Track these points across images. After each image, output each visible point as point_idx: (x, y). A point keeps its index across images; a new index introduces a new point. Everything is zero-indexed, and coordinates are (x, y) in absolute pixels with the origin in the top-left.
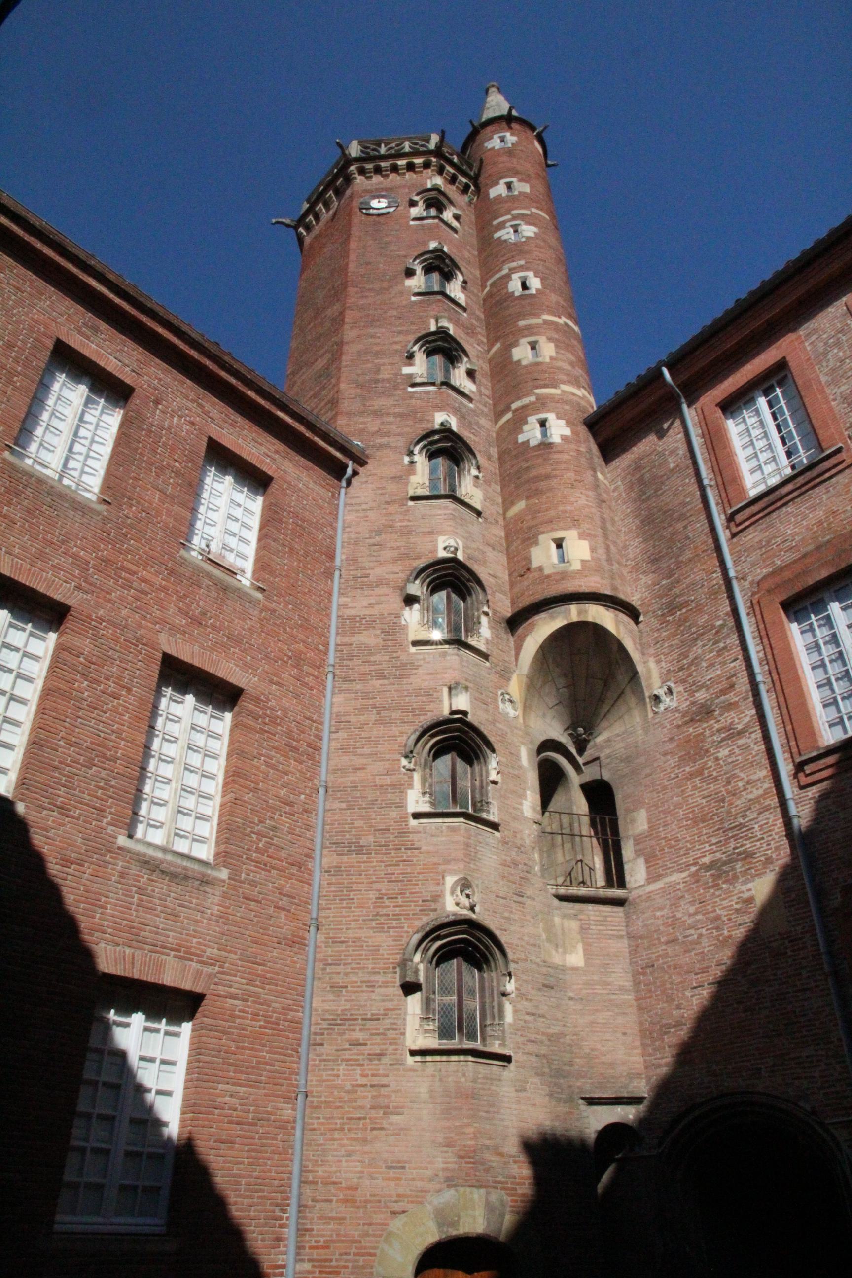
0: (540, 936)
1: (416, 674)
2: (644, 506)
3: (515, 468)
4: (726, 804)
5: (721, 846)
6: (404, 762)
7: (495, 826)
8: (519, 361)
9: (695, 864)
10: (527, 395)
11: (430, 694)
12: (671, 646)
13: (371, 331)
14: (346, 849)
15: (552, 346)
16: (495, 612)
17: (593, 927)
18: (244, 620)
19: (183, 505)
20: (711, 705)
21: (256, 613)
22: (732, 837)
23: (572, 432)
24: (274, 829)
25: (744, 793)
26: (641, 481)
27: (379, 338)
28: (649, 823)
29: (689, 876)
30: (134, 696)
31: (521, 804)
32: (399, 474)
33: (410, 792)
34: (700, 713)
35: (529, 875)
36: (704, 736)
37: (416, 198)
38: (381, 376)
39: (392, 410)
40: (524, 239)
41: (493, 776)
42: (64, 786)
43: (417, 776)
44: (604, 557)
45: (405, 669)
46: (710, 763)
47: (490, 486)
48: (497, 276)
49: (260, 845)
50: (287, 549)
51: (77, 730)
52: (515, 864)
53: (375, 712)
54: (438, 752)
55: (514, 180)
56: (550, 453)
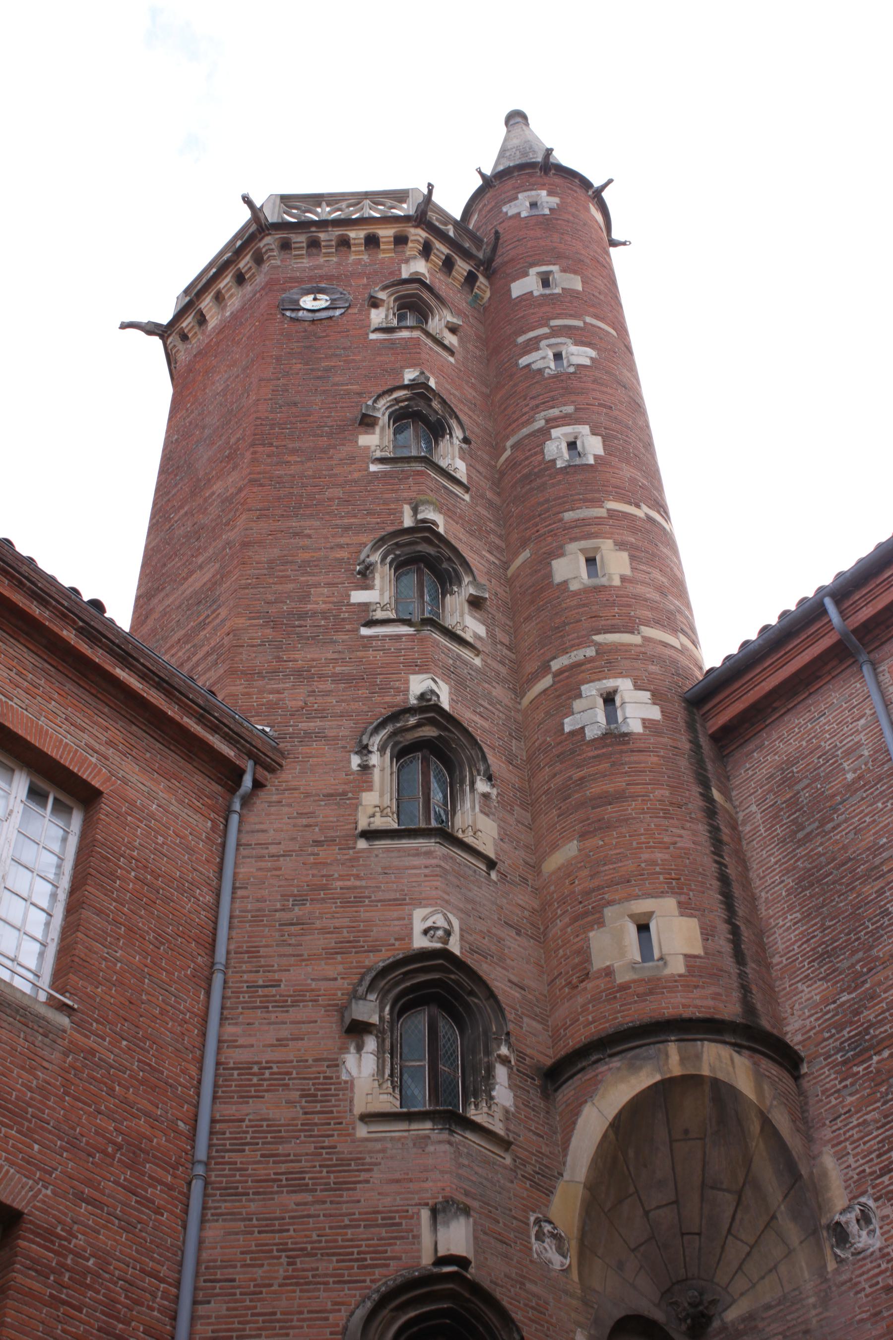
1: (367, 1182)
3: (559, 780)
8: (566, 582)
11: (397, 1224)
16: (521, 1056)
18: (31, 1071)
21: (56, 1056)
26: (793, 803)
27: (309, 536)
37: (382, 295)
39: (329, 670)
40: (572, 370)
47: (511, 811)
48: (525, 431)
53: (284, 1260)
55: (555, 268)
56: (622, 752)
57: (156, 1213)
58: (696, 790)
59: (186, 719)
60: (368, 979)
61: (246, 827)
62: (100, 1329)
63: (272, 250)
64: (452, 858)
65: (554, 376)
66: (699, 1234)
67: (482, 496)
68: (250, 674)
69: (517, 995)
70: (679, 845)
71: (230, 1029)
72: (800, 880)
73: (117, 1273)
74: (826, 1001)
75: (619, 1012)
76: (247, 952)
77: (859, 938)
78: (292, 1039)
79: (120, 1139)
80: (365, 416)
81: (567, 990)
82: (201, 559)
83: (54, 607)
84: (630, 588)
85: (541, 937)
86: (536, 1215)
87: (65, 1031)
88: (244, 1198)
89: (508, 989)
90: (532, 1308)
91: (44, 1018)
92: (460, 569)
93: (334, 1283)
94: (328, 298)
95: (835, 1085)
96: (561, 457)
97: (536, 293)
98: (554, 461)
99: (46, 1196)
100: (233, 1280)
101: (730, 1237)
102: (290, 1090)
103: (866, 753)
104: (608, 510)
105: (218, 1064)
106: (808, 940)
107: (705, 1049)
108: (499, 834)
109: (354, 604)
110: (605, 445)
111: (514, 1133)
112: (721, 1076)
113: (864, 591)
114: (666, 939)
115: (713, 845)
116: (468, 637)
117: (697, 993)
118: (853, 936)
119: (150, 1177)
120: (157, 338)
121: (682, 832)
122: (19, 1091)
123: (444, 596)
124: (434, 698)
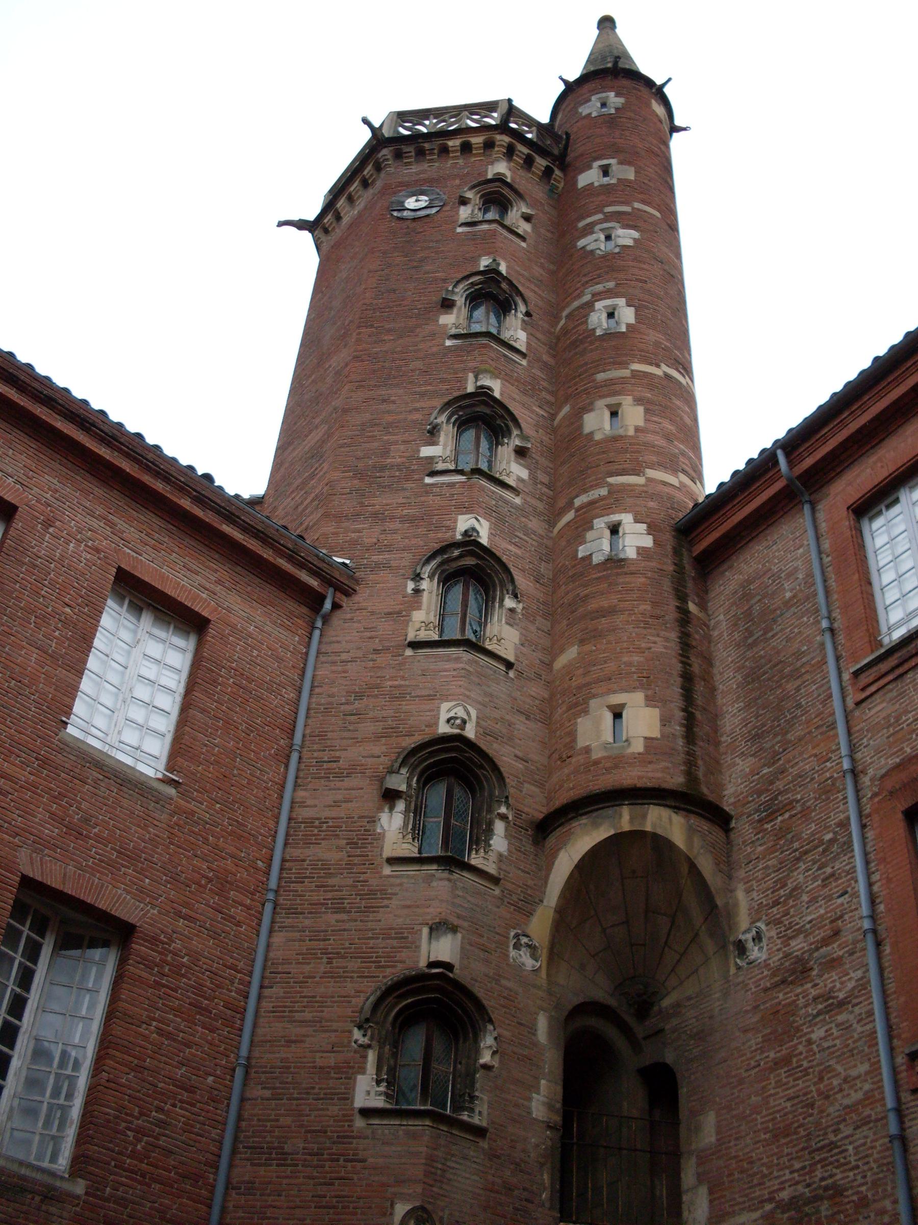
1: (388, 907)
2: (749, 654)
3: (570, 596)
4: (816, 1111)
5: (804, 1175)
6: (357, 1034)
7: (480, 1132)
8: (592, 433)
9: (771, 1200)
11: (405, 938)
12: (767, 867)
13: (383, 392)
14: (264, 1156)
16: (518, 813)
20: (807, 962)
21: (164, 817)
22: (819, 1162)
24: (161, 1124)
25: (839, 1096)
26: (748, 614)
27: (394, 402)
28: (718, 1133)
29: (762, 1217)
31: (530, 1099)
32: (398, 608)
33: (359, 1077)
34: (793, 972)
35: (530, 1205)
36: (797, 1006)
37: (469, 195)
39: (399, 512)
40: (617, 250)
41: (486, 1058)
43: (372, 1056)
45: (372, 898)
46: (800, 1048)
47: (533, 622)
48: (576, 304)
50: (221, 723)
54: (406, 1021)
55: (612, 161)
56: (618, 574)
58: (674, 603)
59: (281, 561)
60: (402, 757)
61: (325, 640)
63: (387, 160)
64: (476, 662)
65: (603, 257)
66: (644, 945)
67: (539, 360)
68: (339, 517)
69: (520, 766)
70: (653, 649)
71: (301, 794)
72: (747, 675)
73: (205, 966)
74: (753, 773)
75: (591, 781)
76: (318, 736)
77: (779, 725)
78: (345, 802)
80: (445, 300)
81: (559, 762)
82: (317, 421)
83: (174, 482)
84: (642, 437)
85: (547, 720)
86: (515, 931)
88: (301, 916)
89: (514, 763)
90: (504, 997)
91: (156, 790)
92: (511, 424)
93: (358, 977)
94: (426, 198)
95: (751, 838)
96: (600, 326)
97: (596, 184)
98: (594, 330)
99: (153, 914)
101: (666, 949)
102: (339, 839)
103: (801, 576)
104: (632, 371)
105: (290, 819)
106: (747, 724)
107: (650, 811)
108: (520, 639)
109: (422, 458)
110: (636, 314)
111: (505, 871)
112: (659, 831)
113: (807, 445)
114: (631, 726)
115: (682, 649)
116: (511, 482)
117: (651, 767)
118: (776, 723)
120: (307, 232)
121: (657, 639)
122: (136, 842)
123: (497, 447)
124: (475, 534)
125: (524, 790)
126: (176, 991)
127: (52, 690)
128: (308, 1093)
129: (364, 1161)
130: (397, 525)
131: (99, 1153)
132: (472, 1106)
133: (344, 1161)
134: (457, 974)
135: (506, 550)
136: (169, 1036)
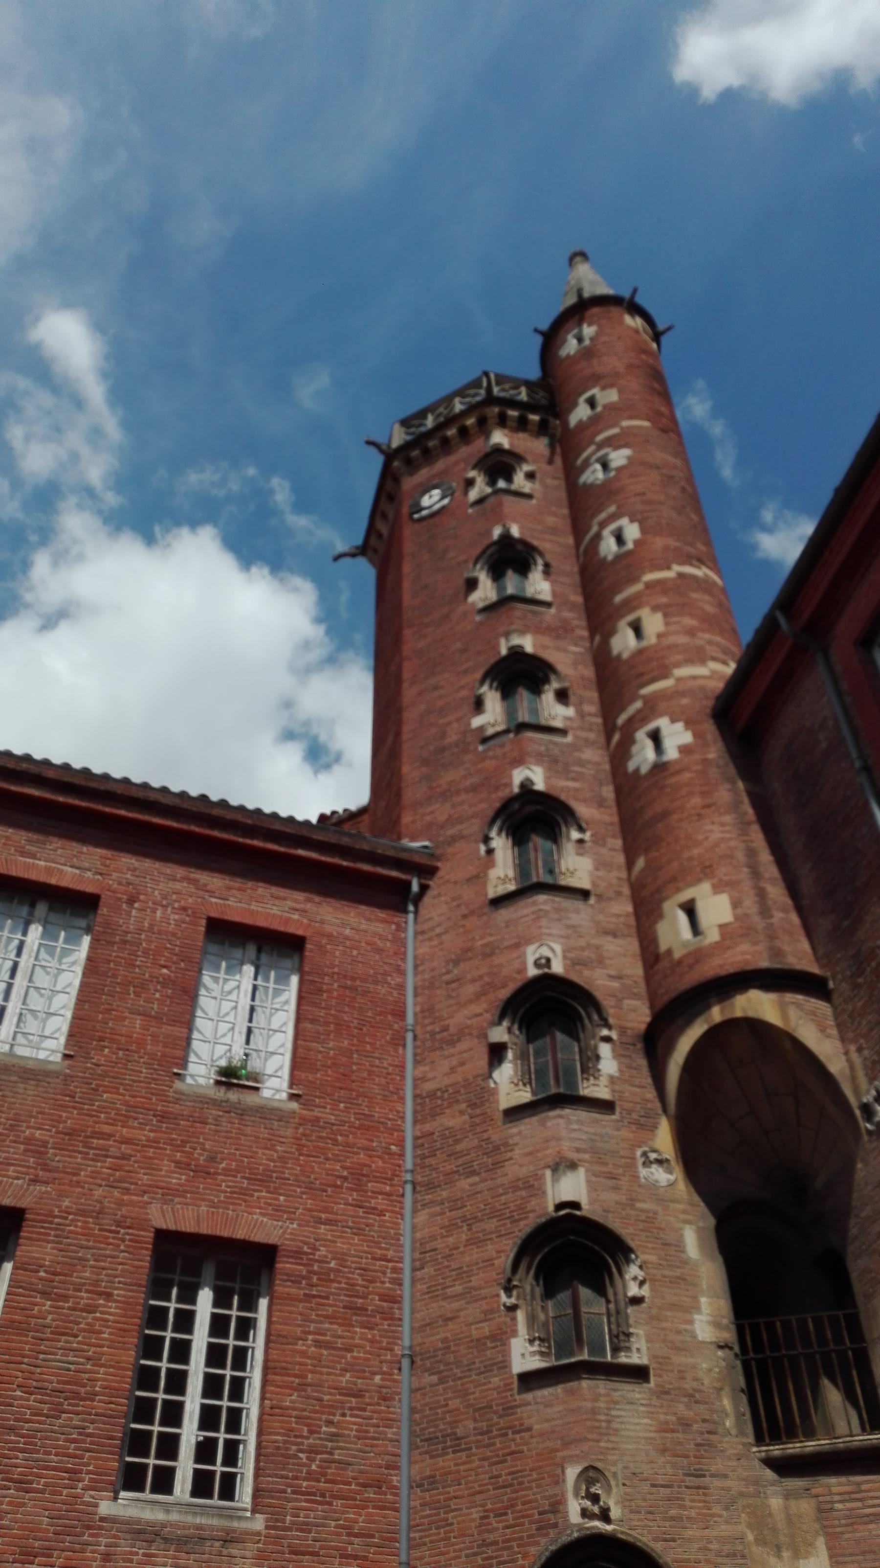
0: (742, 1538)
1: (511, 1159)
7: (640, 1373)
10: (632, 701)
11: (532, 1187)
13: (433, 681)
14: (440, 1446)
15: (658, 617)
16: (623, 1031)
17: (838, 1506)
18: (272, 1148)
19: (173, 1022)
23: (695, 735)
24: (333, 1437)
30: (117, 1301)
31: (691, 1322)
33: (514, 1341)
35: (711, 1437)
38: (447, 741)
41: (633, 1290)
42: (23, 1451)
44: (755, 910)
49: (314, 1467)
51: (38, 1370)
52: (685, 1424)
53: (465, 1228)
55: (595, 391)
57: (379, 1215)
61: (420, 919)
62: (344, 1307)
79: (345, 1173)
87: (294, 1113)
100: (435, 1250)
116: (558, 724)
119: (373, 1192)
125: (625, 1007)
126: (327, 1298)
127: (160, 1048)
128: (470, 1370)
129: (529, 1429)
130: (463, 796)
131: (273, 1483)
132: (627, 1344)
133: (513, 1433)
134: (587, 1209)
135: (565, 788)
136: (328, 1345)
